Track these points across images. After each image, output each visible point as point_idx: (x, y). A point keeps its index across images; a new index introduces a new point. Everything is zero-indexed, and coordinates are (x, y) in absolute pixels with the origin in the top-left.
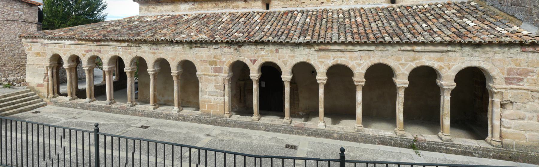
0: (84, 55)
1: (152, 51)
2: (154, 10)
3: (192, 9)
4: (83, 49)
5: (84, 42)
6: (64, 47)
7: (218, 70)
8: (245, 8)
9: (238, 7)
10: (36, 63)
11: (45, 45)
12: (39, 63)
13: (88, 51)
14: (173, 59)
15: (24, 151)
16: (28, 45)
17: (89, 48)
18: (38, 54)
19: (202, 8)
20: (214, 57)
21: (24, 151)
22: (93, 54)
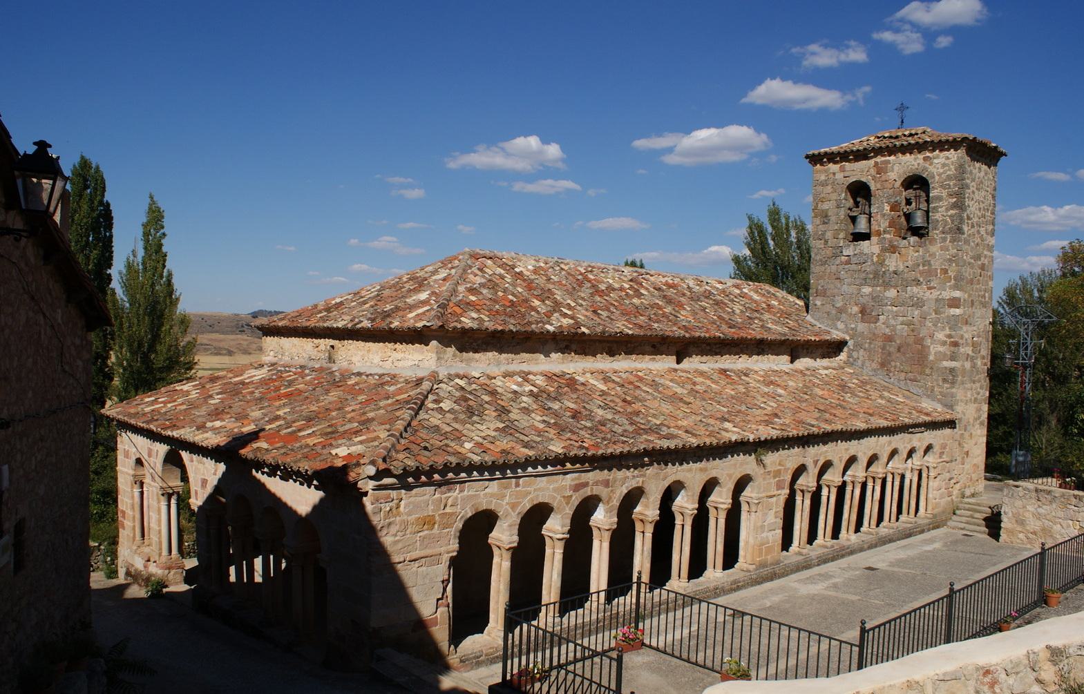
7: (779, 487)
18: (428, 522)
20: (780, 464)
22: (589, 493)
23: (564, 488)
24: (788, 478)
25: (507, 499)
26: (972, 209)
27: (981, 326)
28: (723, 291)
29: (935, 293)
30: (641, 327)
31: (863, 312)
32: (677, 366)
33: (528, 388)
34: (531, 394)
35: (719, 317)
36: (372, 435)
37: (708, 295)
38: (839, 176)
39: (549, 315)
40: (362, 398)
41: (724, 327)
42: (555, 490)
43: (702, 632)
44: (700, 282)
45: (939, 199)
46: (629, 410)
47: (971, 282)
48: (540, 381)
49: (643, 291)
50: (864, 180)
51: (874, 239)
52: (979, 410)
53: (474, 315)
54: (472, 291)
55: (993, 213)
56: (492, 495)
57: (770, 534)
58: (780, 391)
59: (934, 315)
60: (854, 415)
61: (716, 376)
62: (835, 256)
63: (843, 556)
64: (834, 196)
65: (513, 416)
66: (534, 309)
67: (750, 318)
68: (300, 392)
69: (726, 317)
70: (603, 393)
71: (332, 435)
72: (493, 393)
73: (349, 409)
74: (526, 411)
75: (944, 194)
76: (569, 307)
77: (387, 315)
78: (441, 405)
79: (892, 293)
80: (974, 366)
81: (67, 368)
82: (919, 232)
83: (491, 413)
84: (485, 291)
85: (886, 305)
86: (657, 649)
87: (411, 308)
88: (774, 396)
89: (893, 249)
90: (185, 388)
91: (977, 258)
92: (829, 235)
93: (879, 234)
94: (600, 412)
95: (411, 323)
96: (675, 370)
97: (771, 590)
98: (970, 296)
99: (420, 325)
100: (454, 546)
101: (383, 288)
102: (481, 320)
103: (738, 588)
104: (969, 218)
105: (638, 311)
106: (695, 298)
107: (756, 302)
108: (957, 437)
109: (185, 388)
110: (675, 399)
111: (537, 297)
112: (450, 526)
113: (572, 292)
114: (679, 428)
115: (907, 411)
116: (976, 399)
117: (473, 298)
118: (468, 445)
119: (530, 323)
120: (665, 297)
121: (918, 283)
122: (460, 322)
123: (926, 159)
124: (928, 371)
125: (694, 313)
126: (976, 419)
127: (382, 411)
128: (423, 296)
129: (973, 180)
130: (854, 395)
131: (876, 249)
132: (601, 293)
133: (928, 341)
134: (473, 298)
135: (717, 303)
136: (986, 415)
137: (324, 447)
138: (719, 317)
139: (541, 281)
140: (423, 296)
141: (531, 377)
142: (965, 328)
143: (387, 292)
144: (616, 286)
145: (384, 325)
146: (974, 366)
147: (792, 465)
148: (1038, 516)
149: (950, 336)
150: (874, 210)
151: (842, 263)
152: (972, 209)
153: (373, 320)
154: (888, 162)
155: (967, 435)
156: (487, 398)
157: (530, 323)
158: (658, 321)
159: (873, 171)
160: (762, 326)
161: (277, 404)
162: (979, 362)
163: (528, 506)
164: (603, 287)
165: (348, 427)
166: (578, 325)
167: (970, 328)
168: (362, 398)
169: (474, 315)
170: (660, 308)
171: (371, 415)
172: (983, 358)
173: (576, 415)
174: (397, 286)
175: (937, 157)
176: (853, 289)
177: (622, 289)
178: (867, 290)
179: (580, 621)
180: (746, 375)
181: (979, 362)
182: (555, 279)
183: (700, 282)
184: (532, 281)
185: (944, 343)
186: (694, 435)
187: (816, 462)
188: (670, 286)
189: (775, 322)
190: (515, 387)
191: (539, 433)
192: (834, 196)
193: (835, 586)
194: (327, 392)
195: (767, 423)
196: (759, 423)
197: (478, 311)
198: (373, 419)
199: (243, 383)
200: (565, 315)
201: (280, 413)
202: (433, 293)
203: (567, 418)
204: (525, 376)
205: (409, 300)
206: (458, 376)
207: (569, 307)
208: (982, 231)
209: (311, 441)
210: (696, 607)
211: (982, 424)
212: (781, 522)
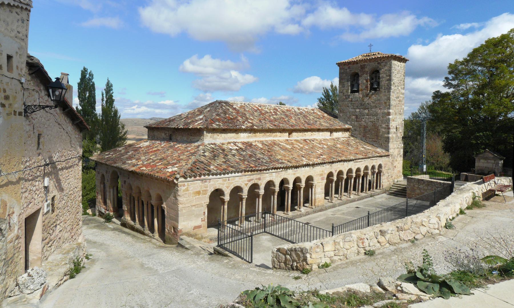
0: (246, 184)
1: (294, 172)
2: (218, 137)
3: (249, 137)
4: (246, 179)
5: (250, 173)
6: (229, 180)
7: (322, 179)
8: (280, 136)
9: (277, 136)
10: (194, 204)
11: (205, 182)
12: (198, 203)
13: (249, 181)
14: (228, 187)
15: (238, 247)
16: (184, 185)
17: (252, 177)
18: (198, 193)
19: (256, 136)
21: (238, 247)
23: (245, 181)
24: (326, 176)
25: (225, 185)
26: (395, 81)
27: (400, 122)
28: (307, 112)
29: (382, 111)
30: (275, 125)
31: (357, 118)
32: (288, 139)
33: (236, 147)
34: (236, 150)
35: (305, 121)
36: (181, 164)
37: (301, 113)
38: (348, 70)
39: (244, 122)
40: (179, 152)
41: (306, 125)
42: (242, 181)
43: (295, 229)
44: (299, 109)
45: (383, 77)
46: (269, 154)
47: (395, 106)
48: (240, 145)
49: (278, 113)
50: (357, 71)
51: (360, 92)
52: (399, 151)
53: (217, 123)
54: (217, 115)
55: (404, 81)
56: (220, 184)
57: (320, 196)
58: (325, 146)
59: (382, 118)
60: (351, 154)
61: (302, 142)
62: (346, 98)
63: (348, 203)
64: (346, 78)
65: (229, 157)
66: (238, 120)
67: (316, 121)
68: (158, 150)
69: (307, 121)
70: (262, 149)
71: (166, 165)
72: (224, 150)
73: (174, 156)
74: (234, 155)
75: (385, 76)
76: (251, 119)
77: (190, 123)
78: (205, 154)
79: (366, 111)
80: (397, 136)
81: (73, 145)
82: (375, 89)
83: (222, 156)
84: (222, 115)
85: (364, 115)
86: (278, 237)
87: (197, 121)
88: (322, 148)
89: (367, 95)
90: (120, 149)
91: (398, 97)
92: (345, 91)
93: (362, 90)
94: (259, 155)
95: (196, 127)
96: (288, 140)
97: (321, 215)
98: (395, 111)
99: (198, 127)
100: (207, 201)
101: (189, 114)
102: (219, 125)
103: (309, 214)
104: (394, 84)
105: (275, 120)
106: (296, 114)
107: (318, 115)
108: (391, 161)
109: (120, 149)
110: (286, 149)
111: (240, 116)
112: (206, 194)
113: (252, 115)
114: (285, 160)
115: (371, 152)
116: (398, 148)
117: (218, 117)
118: (212, 167)
119: (237, 126)
120: (286, 115)
121: (376, 107)
122: (212, 126)
123: (378, 63)
124: (380, 138)
125: (296, 120)
126: (398, 155)
127: (185, 156)
128: (201, 117)
129: (396, 70)
130: (352, 147)
131: (361, 96)
132: (263, 114)
133: (380, 127)
134: (218, 117)
135: (305, 116)
136: (402, 153)
137: (164, 169)
138: (305, 121)
139: (242, 110)
140: (201, 117)
141: (237, 143)
142: (393, 123)
143: (190, 115)
144: (269, 111)
145: (187, 127)
146: (397, 136)
147: (327, 172)
148: (420, 189)
149: (387, 126)
150: (360, 82)
151: (349, 101)
152: (395, 81)
153: (184, 125)
154: (365, 65)
155: (395, 160)
156: (221, 151)
157: (237, 126)
158: (282, 123)
159: (360, 68)
160: (320, 124)
161: (151, 154)
162: (399, 135)
163: (233, 187)
164: (263, 112)
165: (173, 161)
166: (253, 125)
167: (394, 122)
168: (179, 152)
169: (217, 123)
170: (283, 118)
171: (181, 157)
172: (400, 133)
173: (251, 156)
174: (193, 113)
175: (382, 62)
176: (353, 110)
177: (271, 112)
178: (358, 110)
179: (252, 226)
180: (313, 141)
181: (399, 135)
182: (248, 109)
183: (299, 109)
184: (239, 111)
185: (385, 128)
186: (291, 162)
187: (336, 171)
188: (287, 110)
189: (325, 122)
190: (231, 147)
191: (237, 163)
192: (346, 78)
193: (343, 214)
194: (168, 150)
195: (318, 158)
196: (314, 158)
197: (219, 122)
198: (182, 159)
199: (140, 147)
200: (249, 122)
201: (152, 157)
202: (205, 116)
203: (247, 157)
204: (235, 143)
205: (197, 119)
206: (212, 144)
207: (251, 119)
208: (400, 88)
209: (160, 167)
210: (290, 221)
211: (401, 156)
212: (324, 191)
